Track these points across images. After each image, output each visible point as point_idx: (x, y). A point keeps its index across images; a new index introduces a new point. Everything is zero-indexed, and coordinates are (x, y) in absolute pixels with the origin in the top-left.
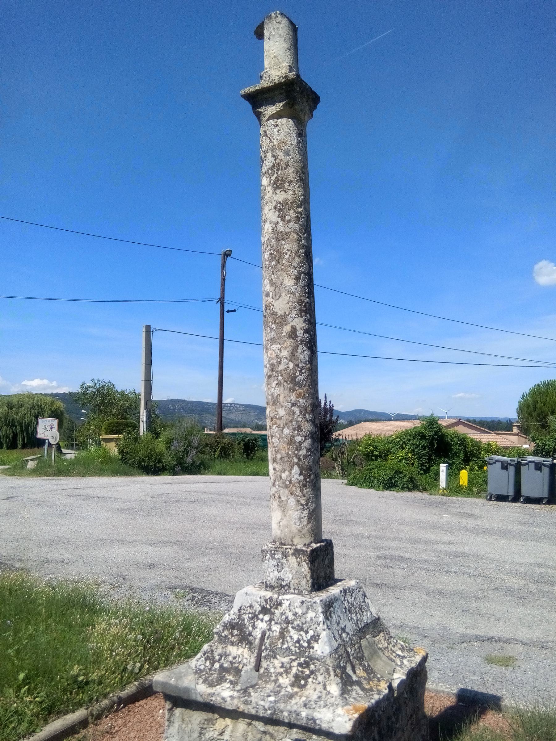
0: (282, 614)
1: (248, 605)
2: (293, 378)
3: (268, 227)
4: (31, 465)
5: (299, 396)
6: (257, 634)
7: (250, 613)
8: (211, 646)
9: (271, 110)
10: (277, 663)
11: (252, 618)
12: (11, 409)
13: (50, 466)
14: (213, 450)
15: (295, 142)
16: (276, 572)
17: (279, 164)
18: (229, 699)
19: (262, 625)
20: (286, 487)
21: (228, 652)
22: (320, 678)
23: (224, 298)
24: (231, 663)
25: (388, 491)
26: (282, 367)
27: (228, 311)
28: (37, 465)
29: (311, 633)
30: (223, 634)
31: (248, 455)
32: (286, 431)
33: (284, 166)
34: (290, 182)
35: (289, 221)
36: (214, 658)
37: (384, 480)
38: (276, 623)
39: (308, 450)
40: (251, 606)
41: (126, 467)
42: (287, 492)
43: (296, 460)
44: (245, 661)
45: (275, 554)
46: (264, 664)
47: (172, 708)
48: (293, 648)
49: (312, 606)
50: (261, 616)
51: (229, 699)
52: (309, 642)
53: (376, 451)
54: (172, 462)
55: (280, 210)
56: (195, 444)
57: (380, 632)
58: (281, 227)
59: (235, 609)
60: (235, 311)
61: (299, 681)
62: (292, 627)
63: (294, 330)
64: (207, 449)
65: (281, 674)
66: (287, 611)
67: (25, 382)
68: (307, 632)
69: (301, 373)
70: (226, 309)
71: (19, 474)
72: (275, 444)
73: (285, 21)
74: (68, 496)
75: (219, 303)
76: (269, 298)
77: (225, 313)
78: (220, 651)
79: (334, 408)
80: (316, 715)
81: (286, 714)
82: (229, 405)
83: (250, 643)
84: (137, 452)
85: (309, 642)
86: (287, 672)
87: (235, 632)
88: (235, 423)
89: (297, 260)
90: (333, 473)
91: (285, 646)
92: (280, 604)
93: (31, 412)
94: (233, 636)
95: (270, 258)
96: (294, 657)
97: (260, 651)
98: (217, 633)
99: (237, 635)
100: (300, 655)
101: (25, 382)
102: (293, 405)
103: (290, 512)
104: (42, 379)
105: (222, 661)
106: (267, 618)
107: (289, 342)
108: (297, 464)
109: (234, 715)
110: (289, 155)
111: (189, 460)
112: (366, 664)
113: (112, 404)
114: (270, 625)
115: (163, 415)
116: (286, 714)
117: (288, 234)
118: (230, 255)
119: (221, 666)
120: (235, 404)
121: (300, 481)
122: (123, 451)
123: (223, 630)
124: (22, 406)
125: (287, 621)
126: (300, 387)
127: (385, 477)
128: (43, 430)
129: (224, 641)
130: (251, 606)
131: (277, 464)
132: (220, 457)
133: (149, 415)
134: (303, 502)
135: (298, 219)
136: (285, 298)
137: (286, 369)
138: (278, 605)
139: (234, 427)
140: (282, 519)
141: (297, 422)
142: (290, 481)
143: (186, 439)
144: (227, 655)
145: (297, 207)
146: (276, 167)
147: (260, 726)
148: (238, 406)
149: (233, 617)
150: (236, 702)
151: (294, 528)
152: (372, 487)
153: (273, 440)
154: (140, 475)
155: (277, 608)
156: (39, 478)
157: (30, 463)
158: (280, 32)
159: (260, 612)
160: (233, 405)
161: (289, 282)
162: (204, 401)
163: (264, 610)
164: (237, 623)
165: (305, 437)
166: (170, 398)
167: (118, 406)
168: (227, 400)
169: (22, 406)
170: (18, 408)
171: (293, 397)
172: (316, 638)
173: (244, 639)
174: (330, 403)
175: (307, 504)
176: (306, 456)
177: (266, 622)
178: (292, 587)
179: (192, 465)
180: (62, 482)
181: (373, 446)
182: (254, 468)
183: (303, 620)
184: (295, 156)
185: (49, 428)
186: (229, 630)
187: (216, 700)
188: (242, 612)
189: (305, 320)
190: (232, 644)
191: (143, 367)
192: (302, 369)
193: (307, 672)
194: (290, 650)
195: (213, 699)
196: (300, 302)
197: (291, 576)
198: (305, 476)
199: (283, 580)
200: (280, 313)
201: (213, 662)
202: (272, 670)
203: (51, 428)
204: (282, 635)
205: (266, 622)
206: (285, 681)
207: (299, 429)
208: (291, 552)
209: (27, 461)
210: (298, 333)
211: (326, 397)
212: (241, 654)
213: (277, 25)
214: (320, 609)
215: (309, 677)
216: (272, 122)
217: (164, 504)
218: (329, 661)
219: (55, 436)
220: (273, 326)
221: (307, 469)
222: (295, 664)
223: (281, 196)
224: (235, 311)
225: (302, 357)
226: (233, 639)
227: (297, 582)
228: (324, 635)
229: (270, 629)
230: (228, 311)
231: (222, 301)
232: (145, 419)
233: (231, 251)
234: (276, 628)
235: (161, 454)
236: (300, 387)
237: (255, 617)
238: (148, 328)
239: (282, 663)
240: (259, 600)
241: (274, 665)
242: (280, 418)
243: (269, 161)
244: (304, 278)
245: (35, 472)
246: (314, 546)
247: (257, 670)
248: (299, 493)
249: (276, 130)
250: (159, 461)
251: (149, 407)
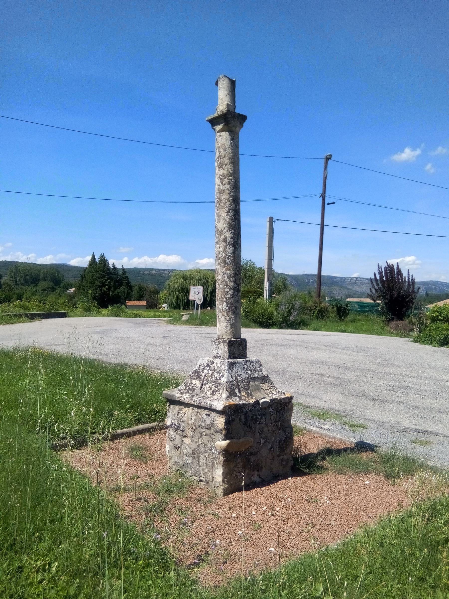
2: (224, 261)
3: (217, 187)
4: (185, 318)
5: (227, 269)
6: (203, 375)
9: (218, 128)
10: (208, 386)
12: (186, 281)
13: (197, 319)
14: (312, 312)
15: (229, 144)
17: (221, 156)
19: (206, 371)
20: (221, 312)
22: (221, 392)
23: (325, 193)
24: (193, 387)
25: (443, 348)
26: (220, 256)
27: (328, 204)
28: (189, 318)
29: (222, 374)
31: (340, 317)
32: (221, 286)
33: (223, 156)
34: (226, 165)
35: (225, 184)
37: (440, 339)
39: (231, 295)
40: (204, 364)
41: (248, 322)
42: (221, 314)
43: (225, 300)
46: (203, 387)
47: (169, 405)
52: (220, 378)
53: (441, 316)
54: (279, 319)
55: (221, 179)
56: (297, 307)
57: (267, 382)
58: (221, 187)
60: (334, 203)
61: (213, 393)
63: (226, 238)
64: (308, 311)
65: (208, 390)
67: (198, 261)
68: (220, 374)
69: (228, 259)
70: (327, 201)
71: (177, 324)
73: (226, 80)
74: (201, 337)
75: (321, 198)
77: (326, 205)
78: (189, 382)
79: (415, 281)
80: (212, 403)
81: (203, 403)
82: (355, 279)
83: (200, 378)
84: (255, 311)
85: (220, 378)
88: (359, 295)
89: (228, 203)
90: (411, 333)
92: (213, 363)
93: (199, 282)
100: (216, 383)
101: (198, 261)
102: (224, 274)
103: (222, 323)
104: (209, 258)
106: (208, 368)
107: (223, 244)
108: (226, 302)
109: (188, 405)
110: (225, 151)
111: (292, 318)
112: (249, 392)
113: (253, 277)
115: (280, 284)
116: (203, 403)
117: (224, 190)
118: (330, 158)
119: (189, 388)
120: (360, 278)
121: (227, 309)
122: (245, 310)
124: (193, 278)
125: (215, 370)
126: (228, 265)
127: (441, 336)
128: (194, 294)
130: (204, 364)
132: (317, 317)
133: (271, 285)
134: (228, 319)
135: (229, 183)
136: (222, 222)
137: (221, 257)
139: (358, 298)
141: (226, 282)
142: (222, 309)
143: (290, 303)
145: (229, 177)
146: (220, 157)
147: (196, 409)
148: (363, 279)
149: (197, 368)
151: (224, 331)
152: (431, 344)
154: (256, 327)
156: (189, 326)
157: (184, 316)
158: (224, 86)
159: (206, 366)
160: (359, 279)
161: (224, 214)
162: (333, 275)
163: (208, 366)
165: (230, 289)
166: (305, 273)
167: (256, 279)
168: (323, 274)
169: (193, 278)
170: (190, 280)
171: (224, 270)
172: (222, 376)
173: (199, 377)
174: (412, 277)
175: (230, 320)
176: (230, 298)
179: (294, 322)
180: (203, 329)
181: (438, 312)
182: (343, 327)
184: (229, 151)
185: (197, 293)
187: (182, 399)
189: (231, 233)
190: (194, 379)
191: (267, 249)
192: (229, 256)
193: (217, 389)
196: (229, 224)
198: (229, 307)
200: (220, 229)
202: (205, 389)
203: (199, 293)
206: (208, 393)
207: (227, 285)
208: (222, 341)
209: (183, 315)
210: (227, 239)
211: (408, 272)
212: (197, 383)
213: (223, 82)
214: (226, 364)
215: (217, 391)
216: (219, 134)
217: (261, 346)
218: (225, 385)
219: (200, 298)
221: (230, 304)
222: (213, 386)
223: (221, 172)
224: (334, 203)
225: (229, 251)
226: (195, 377)
228: (226, 375)
230: (328, 204)
231: (323, 196)
232: (267, 288)
233: (331, 155)
234: (210, 372)
235: (272, 313)
236: (228, 265)
238: (271, 219)
243: (217, 154)
244: (232, 212)
245: (187, 322)
246: (233, 339)
247: (201, 389)
248: (226, 315)
249: (220, 138)
250: (270, 319)
251: (271, 279)
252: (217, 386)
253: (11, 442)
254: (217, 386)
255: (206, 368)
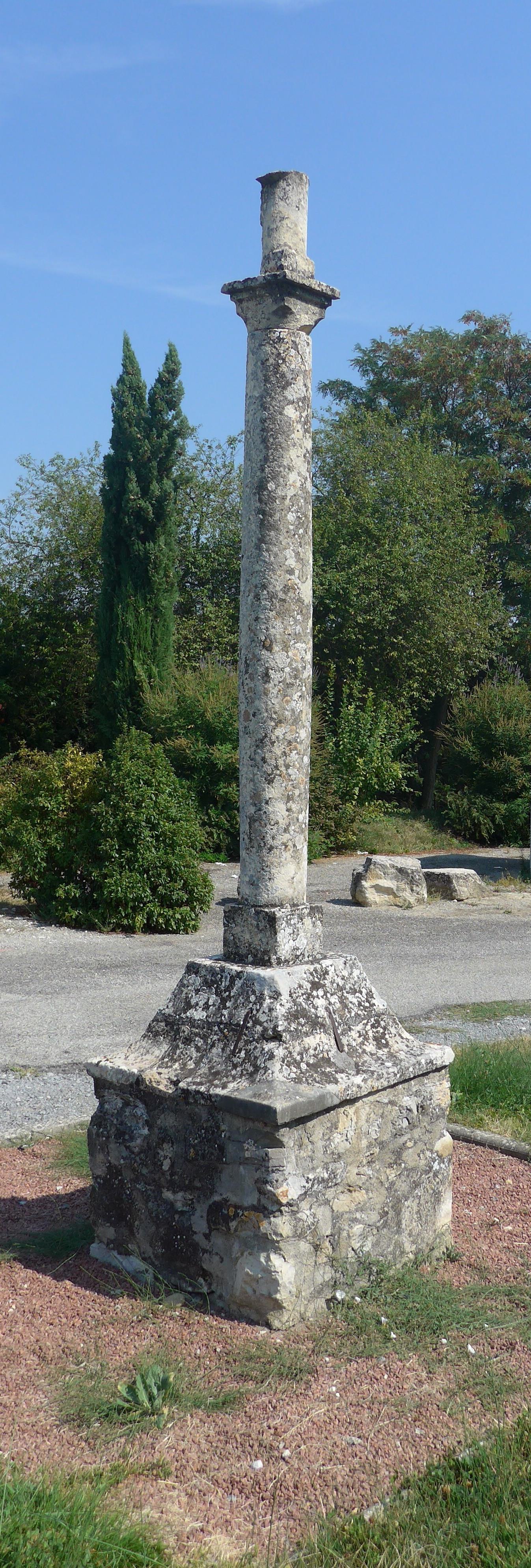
0: (332, 983)
1: (296, 986)
6: (322, 1012)
7: (303, 995)
8: (286, 1048)
10: (354, 1034)
11: (308, 999)
16: (291, 941)
18: (362, 1084)
21: (307, 1046)
30: (292, 1029)
36: (295, 1060)
38: (332, 995)
44: (326, 1047)
45: (290, 919)
46: (344, 1041)
48: (360, 1012)
49: (354, 964)
50: (315, 993)
51: (362, 1084)
59: (285, 997)
62: (347, 993)
65: (362, 1043)
66: (336, 978)
68: (361, 992)
72: (293, 777)
76: (292, 577)
78: (298, 1049)
83: (323, 1026)
86: (366, 1039)
87: (302, 1021)
91: (353, 1014)
92: (327, 973)
94: (302, 1026)
95: (297, 523)
96: (365, 1021)
97: (335, 1029)
98: (284, 1031)
99: (305, 1023)
100: (369, 1017)
105: (305, 1059)
106: (321, 992)
114: (327, 998)
123: (289, 1024)
125: (341, 989)
129: (297, 1035)
130: (300, 986)
131: (294, 802)
138: (324, 974)
140: (296, 873)
144: (306, 1050)
149: (288, 1005)
150: (369, 1082)
153: (290, 771)
155: (325, 979)
159: (312, 989)
163: (315, 986)
164: (297, 1011)
173: (315, 1024)
177: (322, 997)
178: (306, 955)
183: (352, 981)
186: (294, 1022)
188: (294, 995)
190: (307, 1034)
193: (382, 1031)
194: (359, 1015)
195: (350, 1092)
197: (305, 941)
199: (298, 949)
201: (297, 1065)
202: (354, 1044)
204: (345, 1006)
205: (322, 997)
208: (306, 911)
220: (299, 617)
222: (369, 1027)
227: (311, 947)
229: (330, 1004)
234: (334, 999)
237: (309, 997)
239: (359, 1032)
240: (305, 976)
241: (352, 1038)
242: (301, 742)
252: (377, 1022)
253: (83, 782)
254: (377, 1022)
255: (315, 993)
